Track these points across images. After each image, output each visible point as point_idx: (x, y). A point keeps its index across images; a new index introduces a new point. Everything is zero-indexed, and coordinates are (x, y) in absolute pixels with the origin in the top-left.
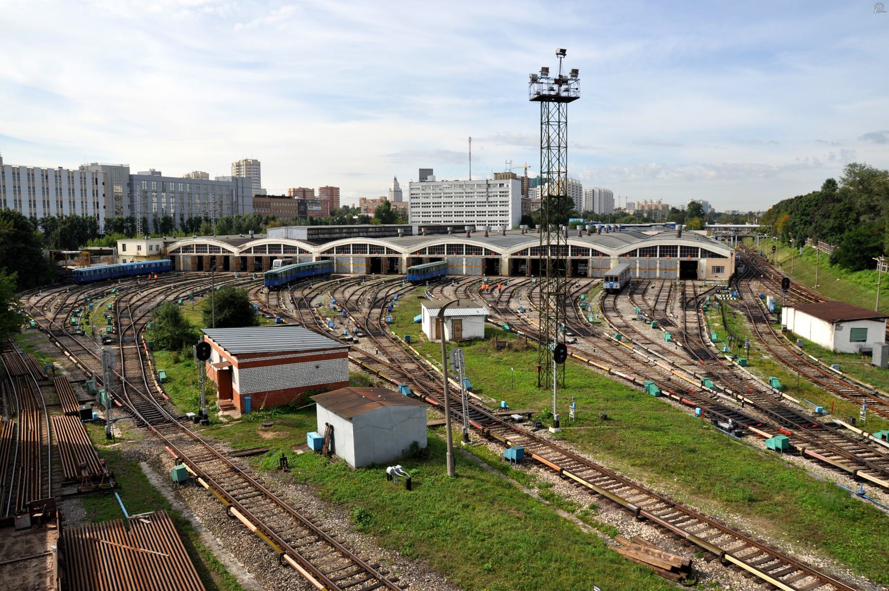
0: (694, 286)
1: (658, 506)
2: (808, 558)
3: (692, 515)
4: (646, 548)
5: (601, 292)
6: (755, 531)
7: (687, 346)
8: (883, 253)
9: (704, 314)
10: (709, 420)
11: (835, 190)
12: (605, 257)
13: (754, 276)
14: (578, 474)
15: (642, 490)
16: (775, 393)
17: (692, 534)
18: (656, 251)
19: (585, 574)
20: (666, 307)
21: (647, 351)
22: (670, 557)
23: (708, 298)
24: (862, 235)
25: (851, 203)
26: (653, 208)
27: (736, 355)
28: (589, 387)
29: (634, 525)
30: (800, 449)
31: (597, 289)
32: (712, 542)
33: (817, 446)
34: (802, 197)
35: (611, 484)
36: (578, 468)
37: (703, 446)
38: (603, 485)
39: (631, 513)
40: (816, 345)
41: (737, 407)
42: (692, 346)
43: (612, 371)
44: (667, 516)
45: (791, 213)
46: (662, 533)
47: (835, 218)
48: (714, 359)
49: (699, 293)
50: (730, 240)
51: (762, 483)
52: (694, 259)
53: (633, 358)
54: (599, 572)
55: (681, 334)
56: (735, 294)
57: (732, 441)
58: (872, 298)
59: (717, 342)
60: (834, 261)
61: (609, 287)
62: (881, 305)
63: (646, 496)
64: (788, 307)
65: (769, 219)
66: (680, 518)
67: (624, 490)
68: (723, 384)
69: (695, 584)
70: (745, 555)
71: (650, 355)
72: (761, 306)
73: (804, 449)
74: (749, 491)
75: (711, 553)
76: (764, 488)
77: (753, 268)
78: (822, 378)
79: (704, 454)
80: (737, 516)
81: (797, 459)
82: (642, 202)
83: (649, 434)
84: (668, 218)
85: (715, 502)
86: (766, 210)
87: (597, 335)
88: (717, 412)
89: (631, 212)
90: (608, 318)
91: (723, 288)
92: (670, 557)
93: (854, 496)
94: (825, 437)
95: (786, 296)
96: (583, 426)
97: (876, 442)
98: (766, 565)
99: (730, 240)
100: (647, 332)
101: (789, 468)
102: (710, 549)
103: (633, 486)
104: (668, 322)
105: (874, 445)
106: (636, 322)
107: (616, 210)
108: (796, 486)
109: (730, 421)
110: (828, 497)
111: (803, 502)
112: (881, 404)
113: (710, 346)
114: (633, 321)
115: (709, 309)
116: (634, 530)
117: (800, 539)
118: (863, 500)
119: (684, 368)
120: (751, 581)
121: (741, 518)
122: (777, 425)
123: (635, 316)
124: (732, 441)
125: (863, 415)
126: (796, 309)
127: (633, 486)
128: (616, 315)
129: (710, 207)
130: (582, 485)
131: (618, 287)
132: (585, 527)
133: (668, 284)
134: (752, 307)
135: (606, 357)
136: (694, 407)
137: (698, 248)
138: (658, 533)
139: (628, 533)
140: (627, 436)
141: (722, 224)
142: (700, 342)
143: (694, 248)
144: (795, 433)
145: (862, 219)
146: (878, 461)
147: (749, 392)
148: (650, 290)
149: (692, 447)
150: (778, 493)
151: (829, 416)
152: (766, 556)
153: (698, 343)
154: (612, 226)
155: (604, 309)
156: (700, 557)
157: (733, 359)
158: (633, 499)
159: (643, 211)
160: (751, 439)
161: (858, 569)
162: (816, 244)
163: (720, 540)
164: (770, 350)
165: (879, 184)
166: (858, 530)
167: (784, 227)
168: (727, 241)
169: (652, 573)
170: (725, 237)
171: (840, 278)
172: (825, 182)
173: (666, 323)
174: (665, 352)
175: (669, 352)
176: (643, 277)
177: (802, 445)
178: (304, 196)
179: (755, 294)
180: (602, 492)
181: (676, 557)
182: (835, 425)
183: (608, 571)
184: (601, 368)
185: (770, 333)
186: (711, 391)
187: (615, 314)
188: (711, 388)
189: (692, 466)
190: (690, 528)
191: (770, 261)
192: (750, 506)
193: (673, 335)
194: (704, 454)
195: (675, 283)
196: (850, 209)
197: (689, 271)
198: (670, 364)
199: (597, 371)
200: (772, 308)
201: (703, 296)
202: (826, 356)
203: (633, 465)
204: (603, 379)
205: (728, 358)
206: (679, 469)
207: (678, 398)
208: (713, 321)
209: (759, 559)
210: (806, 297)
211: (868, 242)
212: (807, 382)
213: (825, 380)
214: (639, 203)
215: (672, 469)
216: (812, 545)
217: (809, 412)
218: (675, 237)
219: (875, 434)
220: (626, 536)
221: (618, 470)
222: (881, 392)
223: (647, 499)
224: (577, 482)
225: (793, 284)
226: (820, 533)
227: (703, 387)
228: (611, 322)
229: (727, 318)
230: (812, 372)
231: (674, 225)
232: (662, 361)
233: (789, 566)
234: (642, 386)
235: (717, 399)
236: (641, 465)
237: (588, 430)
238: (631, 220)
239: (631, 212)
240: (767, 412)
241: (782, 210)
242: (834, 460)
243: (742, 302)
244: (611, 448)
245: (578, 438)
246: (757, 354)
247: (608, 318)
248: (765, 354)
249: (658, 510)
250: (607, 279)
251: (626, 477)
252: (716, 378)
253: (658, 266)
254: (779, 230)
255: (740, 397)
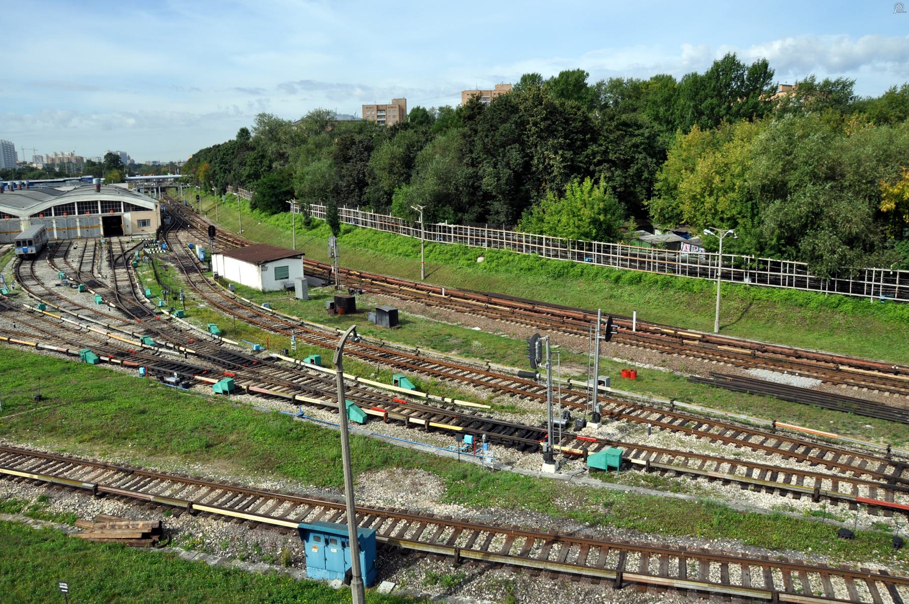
0: (121, 243)
1: (116, 477)
2: (265, 485)
3: (153, 476)
4: (111, 523)
5: (14, 259)
6: (217, 474)
7: (121, 306)
8: (294, 196)
9: (135, 271)
10: (154, 378)
11: (248, 139)
12: (13, 219)
13: (181, 227)
14: (18, 467)
15: (95, 465)
16: (215, 339)
17: (156, 495)
18: (74, 209)
19: (46, 574)
20: (93, 267)
21: (77, 317)
22: (138, 525)
23: (137, 254)
24: (275, 180)
25: (263, 151)
26: (66, 161)
27: (172, 308)
28: (14, 368)
29: (93, 504)
30: (245, 387)
31: (8, 256)
32: (177, 497)
33: (259, 381)
34: (219, 146)
35: (59, 468)
36: (16, 460)
37: (153, 405)
38: (50, 472)
39: (89, 493)
40: (247, 287)
41: (180, 360)
42: (127, 305)
43: (39, 345)
44: (127, 485)
45: (210, 162)
46: (125, 503)
47: (251, 165)
48: (151, 315)
49: (127, 249)
50: (153, 192)
51: (215, 427)
52: (117, 214)
53: (62, 327)
54: (63, 566)
55: (112, 294)
56: (164, 247)
57: (181, 394)
58: (289, 237)
59: (152, 297)
60: (254, 206)
61: (22, 253)
62: (297, 244)
63: (102, 470)
64: (217, 253)
65: (190, 168)
66: (142, 483)
67: (75, 472)
68: (163, 339)
69: (169, 543)
70: (211, 499)
71: (81, 322)
72: (191, 256)
73: (248, 386)
74: (206, 438)
75: (179, 507)
76: (218, 432)
77: (179, 218)
78: (255, 317)
79: (155, 413)
80: (197, 465)
81: (243, 397)
82: (52, 155)
83: (93, 405)
84: (84, 172)
85: (174, 457)
86: (187, 159)
87: (17, 308)
88: (161, 368)
89: (40, 167)
90: (26, 287)
91: (152, 242)
92: (138, 525)
93: (296, 419)
94: (265, 371)
95: (214, 244)
96: (14, 413)
97: (307, 367)
98: (232, 503)
99: (153, 192)
100: (75, 297)
101: (238, 408)
102: (177, 504)
103: (85, 463)
104: (96, 283)
105: (305, 369)
106: (61, 288)
107: (20, 164)
108: (246, 422)
109: (175, 374)
110: (274, 425)
111: (255, 435)
112: (307, 332)
113: (145, 302)
114: (57, 288)
115: (139, 264)
116: (95, 509)
117: (257, 469)
118: (303, 420)
119: (120, 329)
120: (221, 522)
121: (201, 466)
122: (221, 369)
123: (59, 282)
124: (181, 394)
125: (294, 345)
126: (225, 255)
127: (85, 463)
128: (36, 283)
129: (129, 158)
130: (24, 478)
131: (34, 252)
132: (37, 524)
133: (91, 243)
134: (183, 257)
135: (30, 331)
136: (137, 367)
137: (120, 202)
138: (121, 505)
139: (89, 514)
140: (69, 412)
141: (142, 175)
142: (134, 300)
143: (116, 202)
144: (239, 373)
145: (274, 165)
146: (310, 383)
147: (190, 343)
148: (72, 252)
149: (142, 408)
150: (231, 433)
151: (266, 351)
152: (230, 494)
153: (132, 301)
154: (17, 182)
155: (19, 278)
156: (168, 515)
157: (170, 312)
158: (86, 477)
159: (53, 164)
160: (199, 387)
161: (307, 480)
162: (237, 191)
163: (186, 493)
164: (204, 298)
165: (285, 133)
166: (302, 447)
167: (205, 175)
168: (150, 193)
169: (123, 547)
170: (148, 190)
171: (261, 222)
172: (239, 131)
173: (94, 284)
174: (98, 315)
175: (103, 314)
176: (62, 237)
177: (246, 383)
178: (73, 228)
179: (184, 245)
180: (49, 480)
181: (144, 523)
182: (271, 359)
183: (73, 561)
184: (25, 345)
185: (203, 282)
186: (153, 348)
187: (34, 282)
188: (151, 345)
189: (145, 427)
190: (154, 490)
191: (195, 210)
192: (207, 452)
193: (104, 296)
194: (155, 413)
195: (99, 241)
196: (263, 157)
197: (113, 227)
198: (105, 327)
199: (21, 348)
200: (202, 257)
201: (132, 252)
202: (256, 297)
203: (80, 442)
204: (31, 357)
205: (165, 312)
206: (131, 434)
207: (119, 362)
208: (145, 276)
209: (224, 499)
210: (233, 242)
211: (281, 187)
212: (243, 323)
213: (258, 319)
214: (47, 157)
215: (124, 436)
216: (268, 472)
217: (248, 352)
218: (93, 192)
219: (305, 360)
220: (87, 518)
221: (64, 451)
222: (306, 322)
223: (103, 473)
224: (17, 476)
225: (219, 231)
226: (273, 459)
227: (144, 345)
228: (30, 292)
229: (159, 272)
230: (245, 313)
231: (91, 179)
232: (95, 326)
233: (252, 497)
234: (78, 356)
235: (159, 355)
236: (91, 440)
237: (21, 416)
238: (40, 176)
239: (40, 167)
240: (209, 359)
241: (202, 159)
242: (275, 390)
243: (172, 254)
244: (53, 430)
245: (10, 428)
246: (193, 304)
247: (26, 287)
248: (201, 302)
249: (117, 481)
250: (19, 244)
251: (75, 456)
252: (156, 334)
253: (78, 224)
254: (201, 179)
255: (182, 349)
